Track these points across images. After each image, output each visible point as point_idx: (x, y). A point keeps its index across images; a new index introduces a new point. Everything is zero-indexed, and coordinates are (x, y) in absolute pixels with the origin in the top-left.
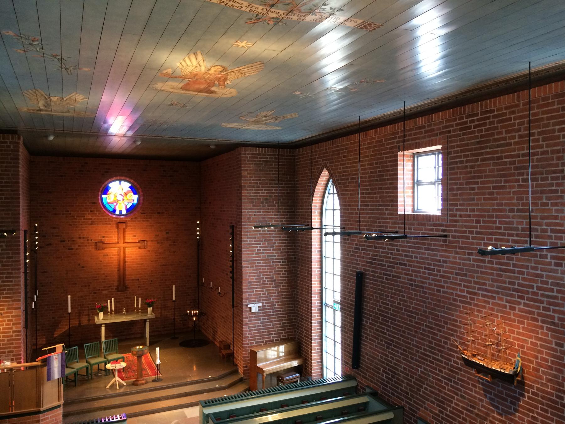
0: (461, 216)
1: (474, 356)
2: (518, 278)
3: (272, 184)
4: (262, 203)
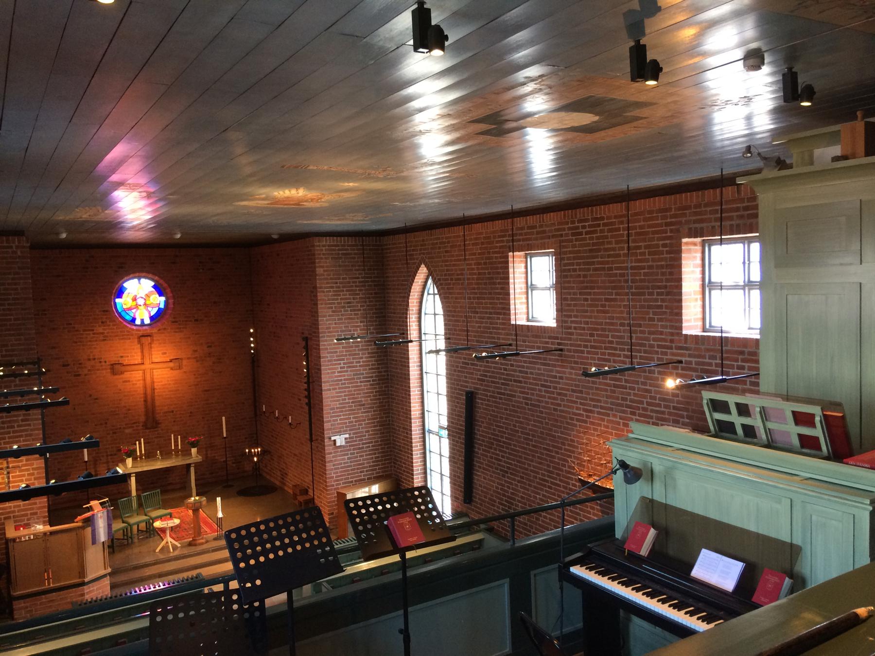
0: (575, 328)
1: (590, 476)
2: (629, 394)
3: (355, 282)
4: (344, 307)
